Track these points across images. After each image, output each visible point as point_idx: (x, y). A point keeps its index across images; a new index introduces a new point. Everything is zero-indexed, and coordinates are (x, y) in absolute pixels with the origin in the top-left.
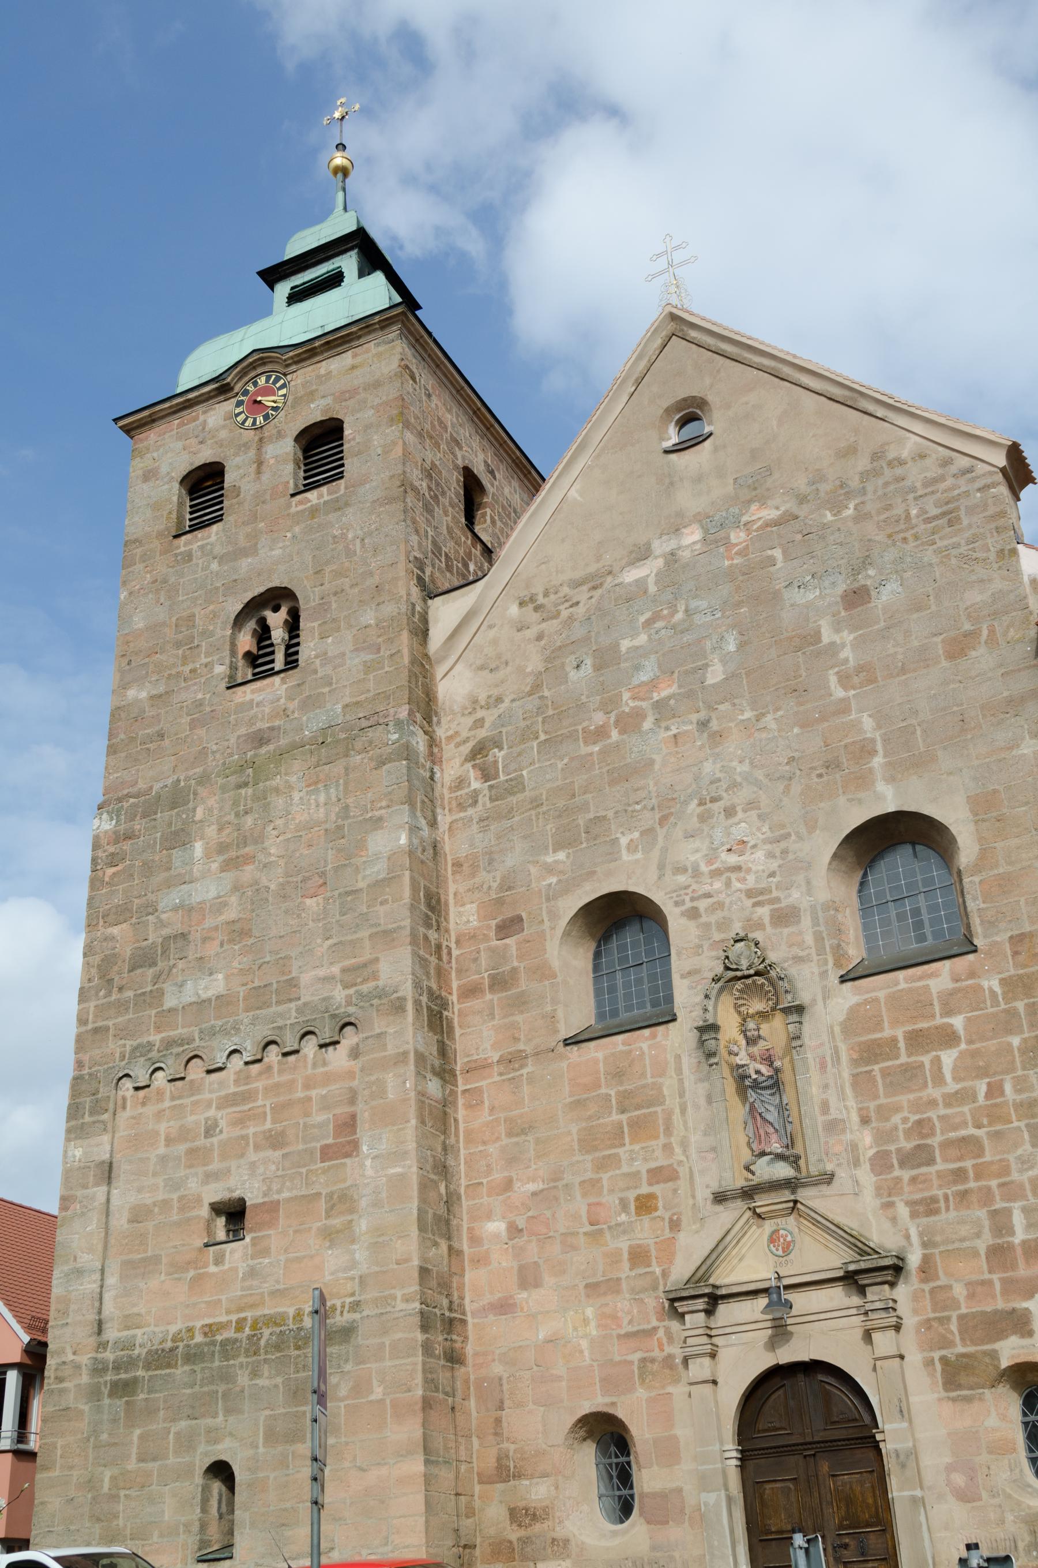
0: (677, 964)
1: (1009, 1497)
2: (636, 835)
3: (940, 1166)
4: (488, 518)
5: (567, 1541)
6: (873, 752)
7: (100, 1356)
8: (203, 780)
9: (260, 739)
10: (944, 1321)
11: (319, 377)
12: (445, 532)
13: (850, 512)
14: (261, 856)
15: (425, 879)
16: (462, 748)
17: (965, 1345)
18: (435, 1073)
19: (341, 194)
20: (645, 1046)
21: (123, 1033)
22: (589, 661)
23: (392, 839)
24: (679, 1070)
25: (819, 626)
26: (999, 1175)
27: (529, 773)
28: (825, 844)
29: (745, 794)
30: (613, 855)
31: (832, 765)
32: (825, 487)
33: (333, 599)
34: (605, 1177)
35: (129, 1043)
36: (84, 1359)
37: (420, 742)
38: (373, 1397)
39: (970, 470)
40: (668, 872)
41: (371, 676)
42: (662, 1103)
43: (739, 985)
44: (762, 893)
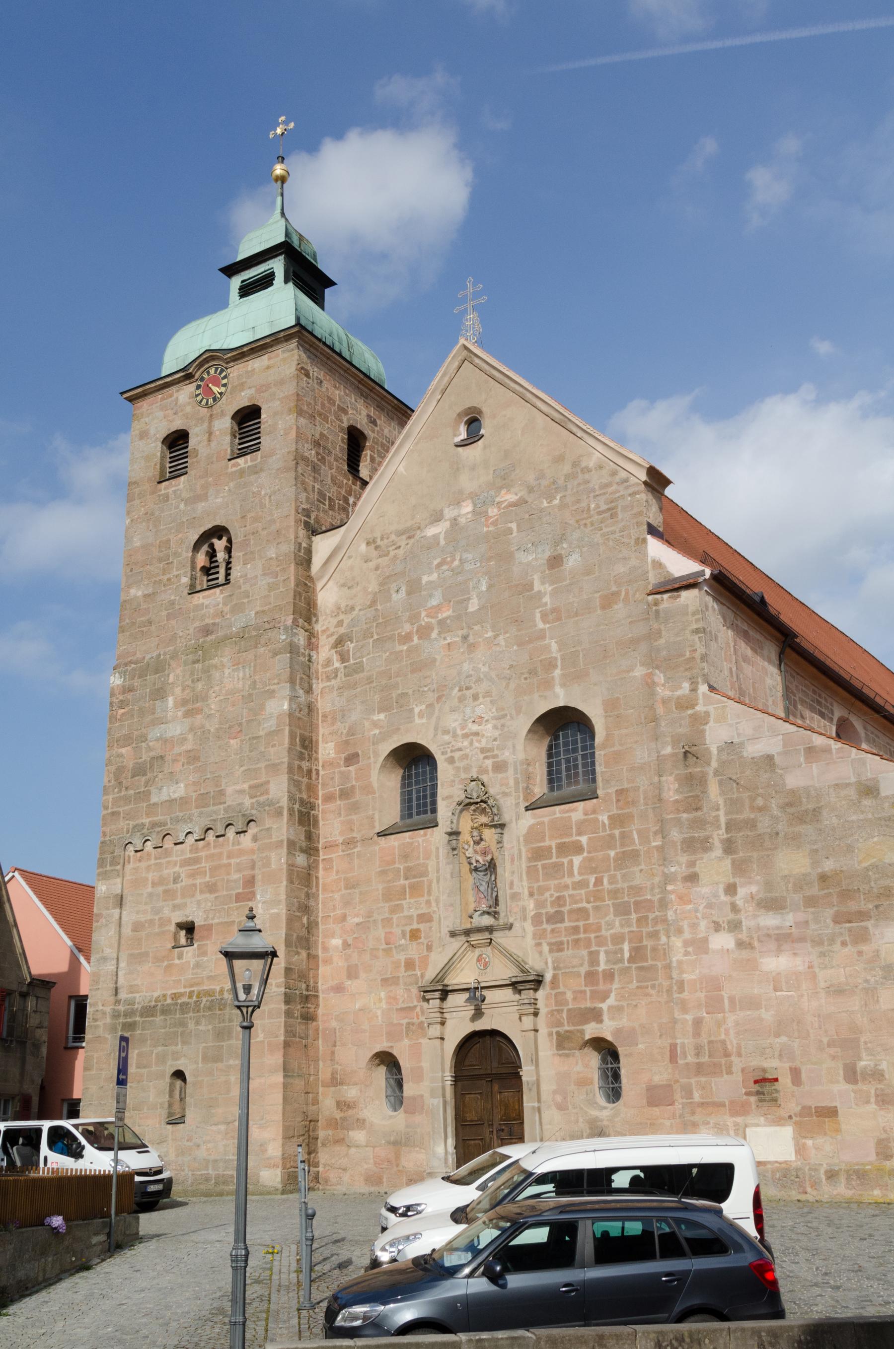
0: (441, 792)
1: (582, 1109)
2: (424, 707)
3: (567, 924)
4: (368, 458)
5: (364, 1120)
6: (555, 667)
7: (116, 1008)
8: (174, 656)
9: (207, 631)
10: (560, 1011)
11: (247, 372)
12: (330, 482)
13: (556, 502)
14: (206, 710)
15: (300, 728)
16: (330, 639)
17: (569, 1026)
18: (302, 851)
19: (279, 199)
20: (420, 840)
21: (129, 816)
22: (404, 588)
23: (279, 705)
24: (437, 857)
25: (533, 579)
26: (595, 932)
27: (367, 660)
28: (525, 723)
29: (485, 686)
30: (410, 719)
31: (533, 672)
32: (544, 483)
33: (252, 537)
34: (395, 917)
35: (131, 823)
36: (108, 1009)
37: (301, 639)
38: (258, 1039)
39: (626, 480)
40: (440, 732)
41: (272, 594)
42: (427, 876)
43: (473, 807)
44: (489, 751)
